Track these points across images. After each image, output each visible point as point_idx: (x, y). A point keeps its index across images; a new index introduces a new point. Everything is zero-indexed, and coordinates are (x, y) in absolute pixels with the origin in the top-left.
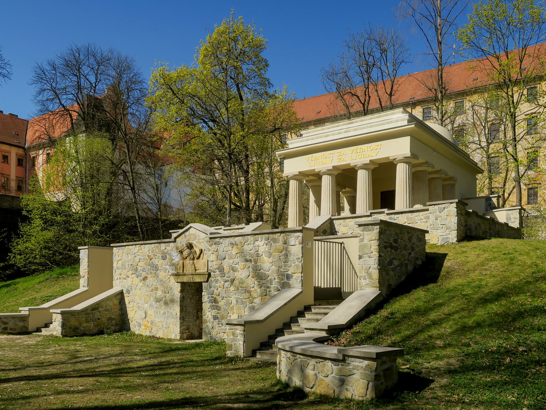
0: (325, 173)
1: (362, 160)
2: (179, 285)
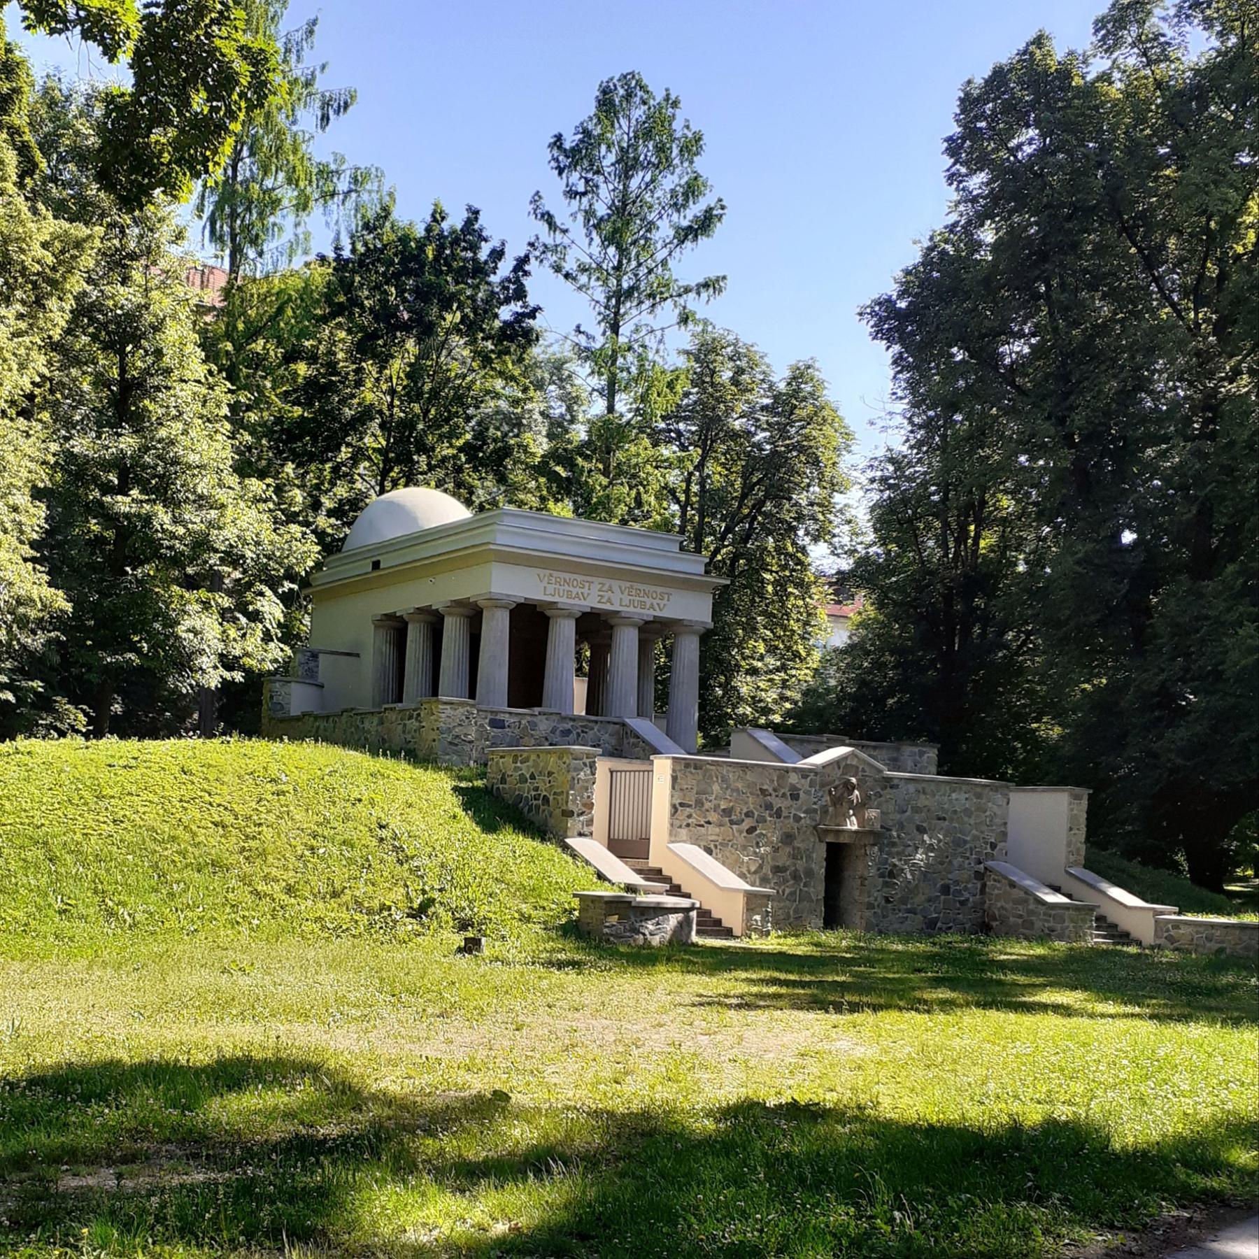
0: (569, 616)
1: (638, 610)
2: (824, 847)
